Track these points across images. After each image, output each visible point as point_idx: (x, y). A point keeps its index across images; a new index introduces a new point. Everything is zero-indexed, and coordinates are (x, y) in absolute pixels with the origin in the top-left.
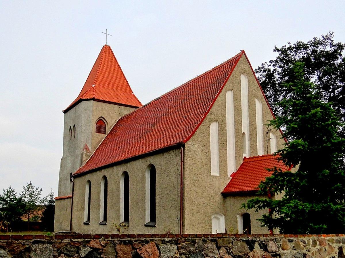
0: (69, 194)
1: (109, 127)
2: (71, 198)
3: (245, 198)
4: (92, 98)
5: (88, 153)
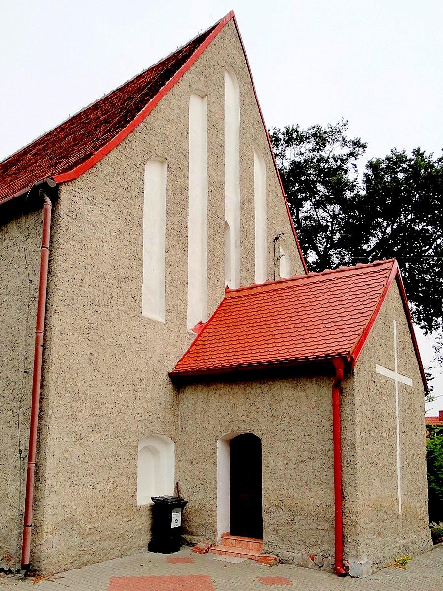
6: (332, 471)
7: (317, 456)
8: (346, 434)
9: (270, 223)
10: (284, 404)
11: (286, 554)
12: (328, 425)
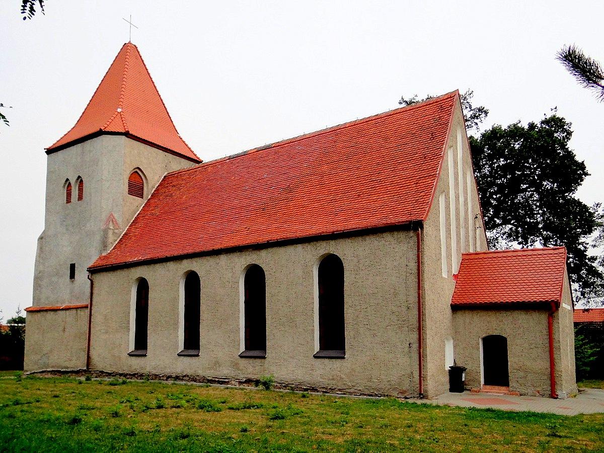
0: (67, 302)
1: (150, 186)
2: (86, 307)
3: (496, 313)
4: (123, 131)
5: (117, 229)
6: (548, 353)
7: (539, 346)
8: (555, 336)
9: (473, 209)
10: (520, 322)
11: (523, 391)
12: (545, 332)
